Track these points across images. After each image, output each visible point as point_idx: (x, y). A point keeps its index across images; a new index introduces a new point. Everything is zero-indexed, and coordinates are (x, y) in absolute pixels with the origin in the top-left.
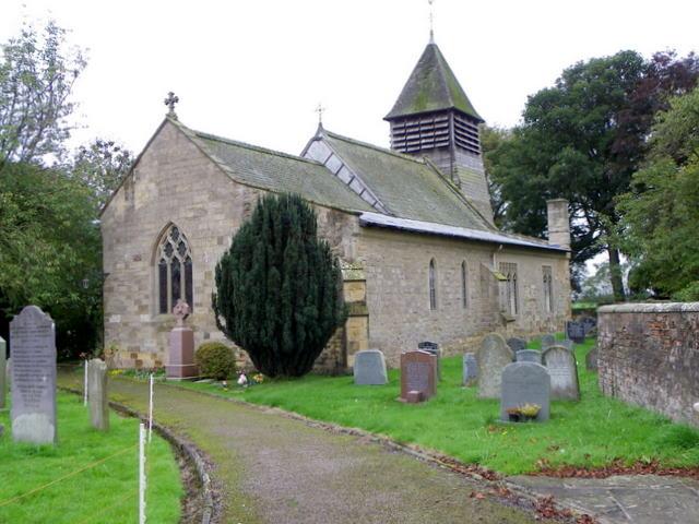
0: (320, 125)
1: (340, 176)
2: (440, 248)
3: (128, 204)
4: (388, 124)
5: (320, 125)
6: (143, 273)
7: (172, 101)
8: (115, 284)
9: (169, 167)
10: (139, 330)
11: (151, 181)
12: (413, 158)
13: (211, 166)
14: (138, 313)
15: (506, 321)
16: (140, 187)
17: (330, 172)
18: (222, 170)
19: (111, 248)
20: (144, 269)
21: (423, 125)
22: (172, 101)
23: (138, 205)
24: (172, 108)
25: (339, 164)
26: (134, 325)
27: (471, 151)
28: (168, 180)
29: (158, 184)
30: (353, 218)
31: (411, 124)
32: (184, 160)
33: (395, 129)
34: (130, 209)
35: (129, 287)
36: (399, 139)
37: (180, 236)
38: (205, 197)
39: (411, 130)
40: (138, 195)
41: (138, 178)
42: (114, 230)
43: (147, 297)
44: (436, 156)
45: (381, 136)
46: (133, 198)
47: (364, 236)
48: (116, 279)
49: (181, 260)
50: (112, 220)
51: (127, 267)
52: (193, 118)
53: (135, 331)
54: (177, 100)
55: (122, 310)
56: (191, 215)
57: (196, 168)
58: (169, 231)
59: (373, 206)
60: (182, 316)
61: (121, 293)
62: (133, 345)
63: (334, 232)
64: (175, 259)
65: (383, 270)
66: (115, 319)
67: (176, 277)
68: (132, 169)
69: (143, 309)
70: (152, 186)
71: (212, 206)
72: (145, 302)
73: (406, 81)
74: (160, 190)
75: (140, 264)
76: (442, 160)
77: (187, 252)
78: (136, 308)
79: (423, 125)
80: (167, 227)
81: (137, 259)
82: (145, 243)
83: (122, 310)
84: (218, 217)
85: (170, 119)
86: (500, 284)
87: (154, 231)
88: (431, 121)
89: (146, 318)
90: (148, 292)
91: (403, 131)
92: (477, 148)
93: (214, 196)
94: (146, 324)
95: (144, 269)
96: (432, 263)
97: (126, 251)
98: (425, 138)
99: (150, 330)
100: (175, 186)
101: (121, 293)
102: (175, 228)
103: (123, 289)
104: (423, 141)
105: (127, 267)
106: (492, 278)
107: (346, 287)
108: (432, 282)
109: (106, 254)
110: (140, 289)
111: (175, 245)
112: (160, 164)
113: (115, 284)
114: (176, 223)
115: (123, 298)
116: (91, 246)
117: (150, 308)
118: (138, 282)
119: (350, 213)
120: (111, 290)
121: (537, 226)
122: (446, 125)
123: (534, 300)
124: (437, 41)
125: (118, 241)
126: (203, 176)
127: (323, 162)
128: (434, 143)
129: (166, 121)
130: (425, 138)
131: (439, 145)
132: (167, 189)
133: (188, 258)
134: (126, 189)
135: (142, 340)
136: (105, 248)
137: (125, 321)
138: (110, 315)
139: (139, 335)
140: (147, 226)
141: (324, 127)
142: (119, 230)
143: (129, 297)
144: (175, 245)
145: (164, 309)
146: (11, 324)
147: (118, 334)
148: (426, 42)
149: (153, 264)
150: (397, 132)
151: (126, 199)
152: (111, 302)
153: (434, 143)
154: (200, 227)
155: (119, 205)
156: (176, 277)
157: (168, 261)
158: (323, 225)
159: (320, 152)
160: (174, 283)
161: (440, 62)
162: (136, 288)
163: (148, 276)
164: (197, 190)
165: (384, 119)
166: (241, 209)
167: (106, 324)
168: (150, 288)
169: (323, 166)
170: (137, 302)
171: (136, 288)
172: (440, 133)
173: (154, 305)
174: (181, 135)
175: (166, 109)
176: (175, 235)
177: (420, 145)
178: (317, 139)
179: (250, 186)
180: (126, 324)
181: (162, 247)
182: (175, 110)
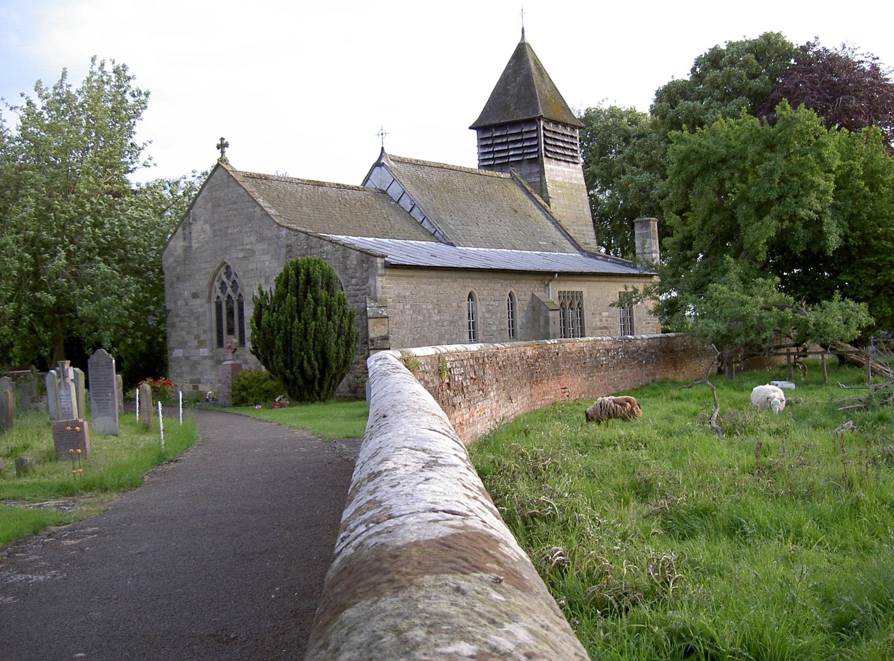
0: (383, 148)
1: (401, 203)
2: (480, 281)
3: (186, 244)
4: (474, 132)
5: (383, 148)
6: (201, 310)
7: (222, 146)
8: (176, 320)
9: (221, 209)
10: (199, 363)
11: (206, 222)
12: (490, 173)
13: (258, 209)
14: (198, 347)
15: (706, 336)
16: (196, 228)
17: (392, 200)
18: (267, 214)
19: (172, 286)
20: (202, 306)
21: (512, 135)
22: (222, 146)
23: (195, 245)
24: (223, 152)
25: (400, 190)
26: (194, 358)
27: (556, 159)
28: (221, 221)
29: (212, 225)
30: (379, 260)
31: (498, 134)
32: (235, 203)
33: (482, 139)
34: (187, 249)
35: (189, 323)
36: (486, 150)
37: (233, 275)
38: (253, 239)
39: (499, 141)
40: (194, 235)
41: (194, 220)
42: (174, 268)
43: (205, 332)
44: (526, 169)
45: (465, 152)
46: (190, 239)
47: (389, 275)
48: (177, 316)
49: (235, 297)
50: (172, 260)
51: (186, 304)
52: (241, 162)
53: (194, 365)
54: (227, 145)
55: (183, 345)
56: (241, 255)
57: (245, 211)
58: (223, 270)
59: (433, 235)
60: (231, 351)
61: (182, 329)
62: (195, 377)
63: (362, 274)
64: (229, 297)
65: (412, 306)
66: (178, 353)
67: (231, 313)
68: (189, 210)
69: (202, 344)
70: (207, 227)
71: (259, 247)
72: (203, 337)
73: (294, 174)
74: (214, 231)
75: (198, 302)
76: (531, 174)
77: (239, 290)
78: (195, 343)
79: (512, 135)
80: (221, 266)
81: (195, 296)
82: (201, 282)
83: (183, 345)
84: (265, 258)
85: (223, 160)
86: (551, 314)
87: (210, 270)
88: (519, 130)
89: (204, 351)
90: (206, 328)
91: (490, 142)
92: (576, 151)
93: (261, 238)
94: (205, 358)
95: (202, 306)
96: (471, 296)
97: (185, 290)
98: (514, 149)
99: (209, 363)
100: (228, 228)
101: (182, 329)
102: (228, 267)
103: (184, 324)
104: (511, 153)
105: (186, 304)
106: (543, 308)
107: (371, 322)
108: (471, 315)
109: (168, 291)
110: (199, 325)
111: (229, 284)
112: (214, 207)
113: (176, 320)
114: (229, 264)
115: (184, 333)
116: (154, 285)
117: (208, 343)
118: (197, 318)
119: (376, 256)
120: (173, 325)
121: (627, 248)
122: (535, 135)
123: (605, 328)
124: (528, 39)
125: (178, 279)
126: (250, 219)
127: (385, 189)
128: (523, 154)
129: (218, 165)
130: (514, 149)
131: (528, 157)
132: (220, 230)
133: (240, 295)
134: (184, 229)
135: (201, 373)
136: (167, 286)
137: (187, 355)
138: (173, 349)
139: (200, 368)
140: (204, 265)
141: (386, 150)
142: (179, 269)
143: (189, 333)
144: (229, 284)
145: (220, 343)
146: (89, 361)
147: (181, 367)
148: (518, 40)
149: (209, 300)
150: (485, 143)
151: (185, 239)
152: (174, 338)
153: (523, 154)
154: (250, 267)
155: (177, 245)
156: (231, 313)
157: (224, 299)
158: (353, 266)
159: (381, 179)
160: (228, 316)
161: (532, 63)
162: (195, 324)
163: (205, 312)
164: (247, 232)
165: (470, 128)
166: (284, 250)
167: (170, 358)
168: (207, 324)
169: (384, 192)
170: (197, 337)
171: (195, 324)
172: (528, 144)
173: (212, 340)
174: (231, 179)
175: (218, 154)
176: (228, 273)
177: (508, 157)
178: (378, 164)
179: (292, 230)
180: (187, 358)
181: (217, 284)
182: (227, 155)
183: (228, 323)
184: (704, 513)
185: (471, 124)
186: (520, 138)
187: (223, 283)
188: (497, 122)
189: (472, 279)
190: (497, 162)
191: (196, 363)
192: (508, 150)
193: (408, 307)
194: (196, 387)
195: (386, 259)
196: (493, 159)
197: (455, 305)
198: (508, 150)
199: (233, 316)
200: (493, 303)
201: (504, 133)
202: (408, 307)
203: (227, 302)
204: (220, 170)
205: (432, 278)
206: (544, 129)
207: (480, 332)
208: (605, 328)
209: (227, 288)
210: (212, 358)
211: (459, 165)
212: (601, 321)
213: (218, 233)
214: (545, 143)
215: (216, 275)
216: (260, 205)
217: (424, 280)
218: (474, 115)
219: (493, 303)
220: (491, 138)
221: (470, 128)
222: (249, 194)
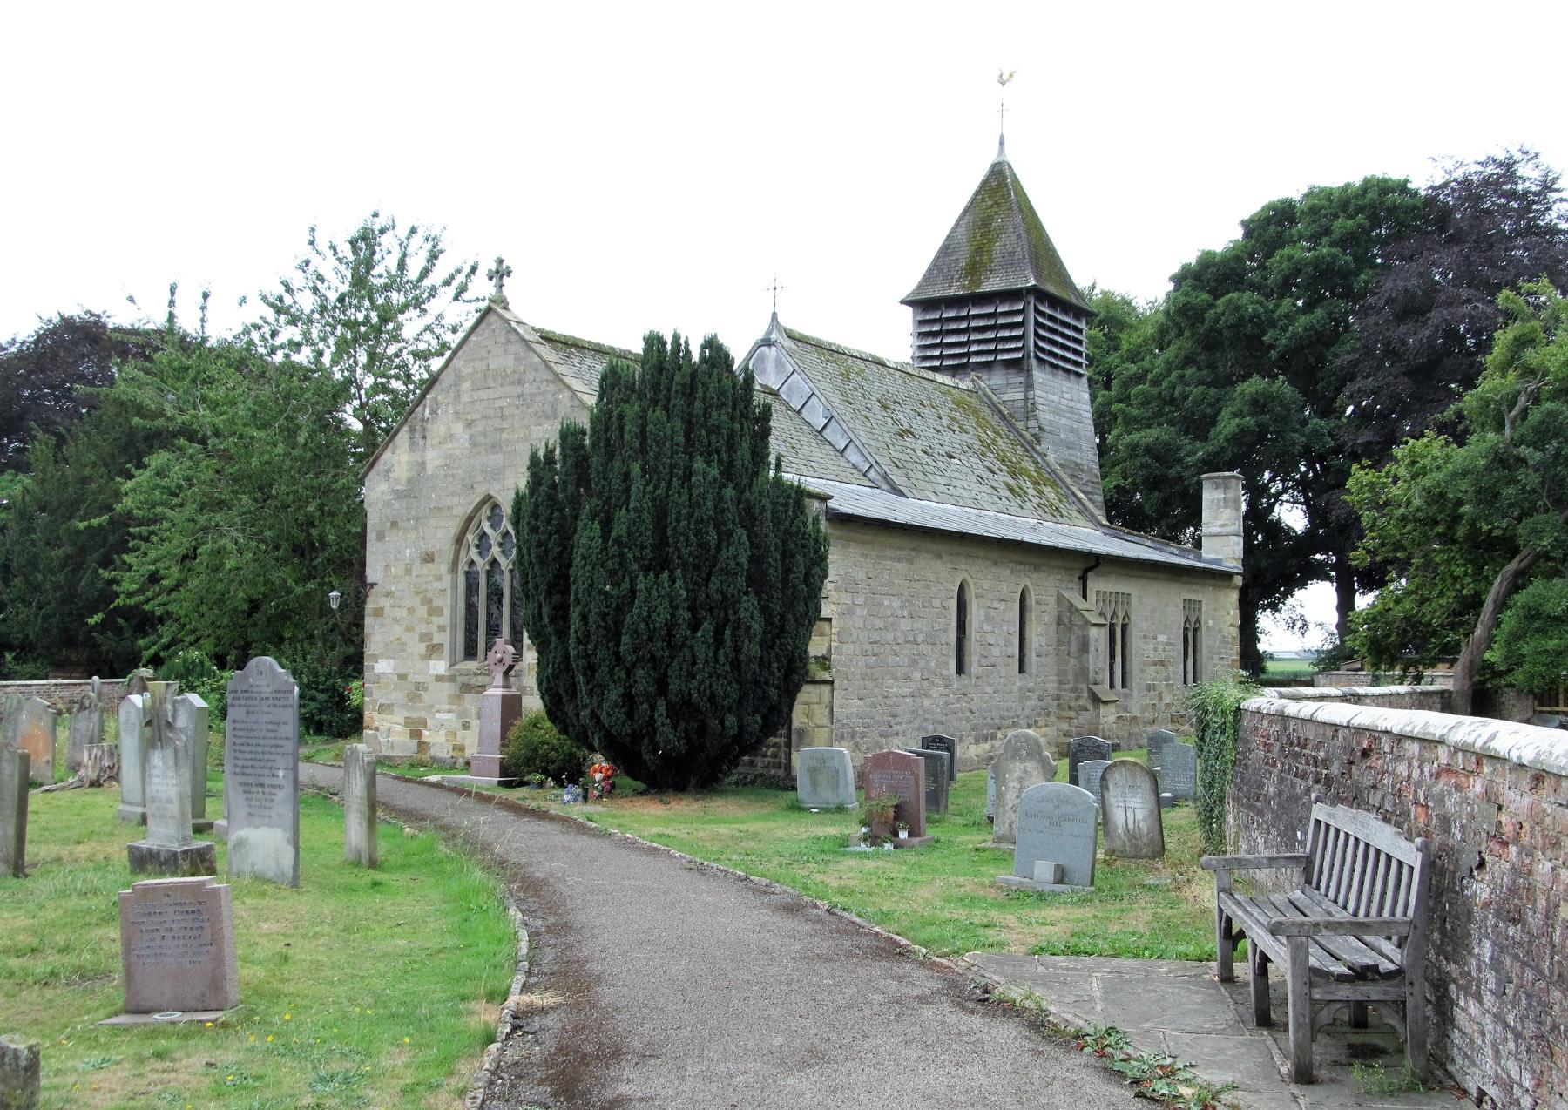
1: (804, 413)
8: (385, 603)
10: (426, 689)
13: (564, 396)
29: (470, 424)
30: (816, 504)
31: (952, 314)
36: (929, 341)
39: (953, 326)
43: (442, 628)
45: (893, 337)
58: (486, 511)
62: (415, 715)
64: (494, 562)
69: (434, 650)
70: (458, 428)
78: (422, 648)
89: (440, 666)
91: (936, 328)
94: (439, 678)
95: (439, 578)
98: (979, 342)
99: (448, 689)
104: (974, 348)
106: (1077, 620)
123: (1162, 663)
124: (1011, 157)
125: (394, 524)
128: (995, 352)
130: (979, 342)
131: (1006, 357)
137: (404, 671)
138: (375, 658)
145: (470, 652)
149: (454, 568)
150: (926, 329)
153: (995, 352)
157: (482, 565)
165: (903, 302)
170: (425, 637)
172: (1007, 334)
174: (513, 337)
177: (968, 355)
181: (471, 538)
183: (489, 615)
184: (485, 848)
185: (903, 296)
186: (991, 322)
187: (484, 535)
188: (951, 292)
189: (969, 556)
190: (946, 363)
191: (419, 686)
192: (968, 343)
193: (860, 600)
194: (416, 734)
195: (830, 504)
196: (940, 357)
197: (936, 603)
198: (968, 343)
199: (500, 601)
200: (996, 604)
201: (964, 313)
202: (860, 600)
203: (490, 574)
204: (492, 318)
205: (900, 548)
206: (1037, 310)
207: (975, 658)
208: (1162, 663)
209: (490, 546)
210: (452, 679)
211: (1258, 208)
212: (1156, 649)
213: (481, 439)
214: (1037, 334)
215: (470, 519)
216: (569, 388)
217: (889, 553)
218: (910, 277)
219: (996, 604)
220: (939, 321)
221: (903, 302)
222: (550, 369)
